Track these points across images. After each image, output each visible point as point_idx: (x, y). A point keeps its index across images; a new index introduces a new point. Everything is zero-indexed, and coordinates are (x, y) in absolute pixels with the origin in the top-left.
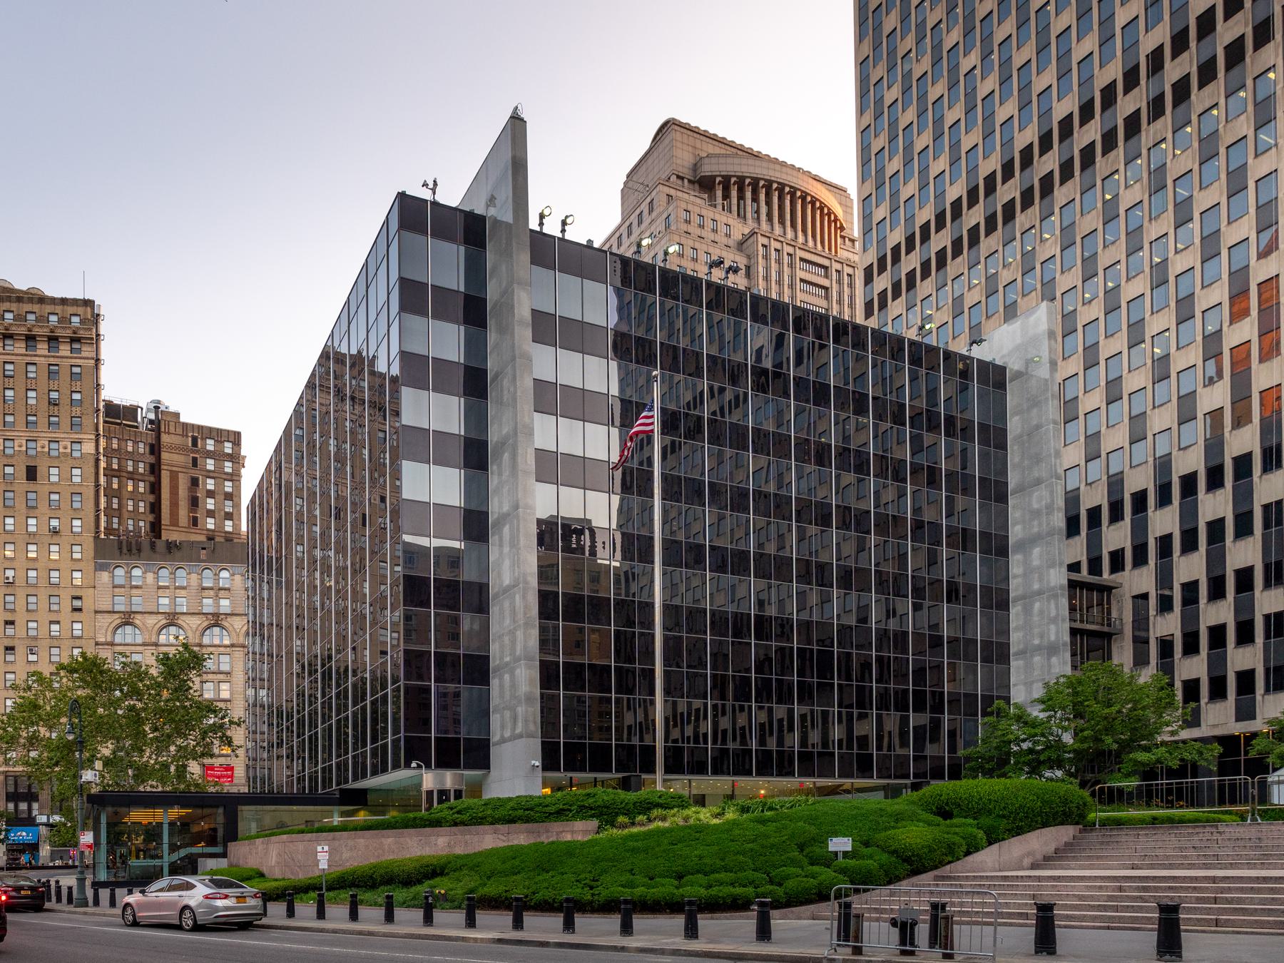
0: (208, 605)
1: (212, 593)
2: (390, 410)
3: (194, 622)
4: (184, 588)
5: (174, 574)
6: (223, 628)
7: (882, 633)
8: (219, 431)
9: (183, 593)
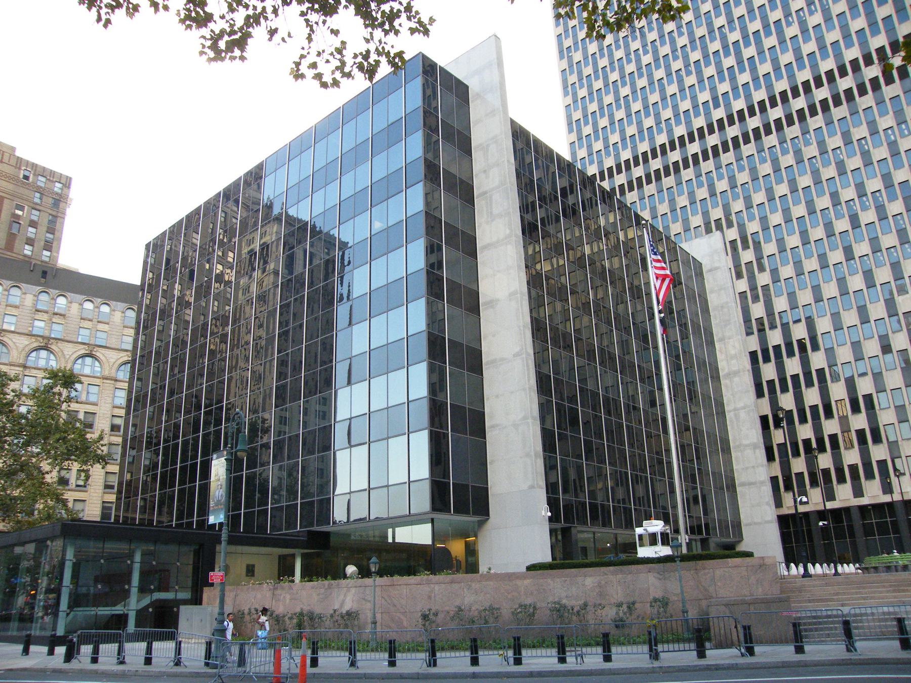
0: (40, 326)
1: (45, 317)
2: (242, 203)
3: (70, 351)
4: (16, 307)
5: (8, 291)
6: (50, 351)
7: (279, 457)
8: (52, 173)
9: (14, 311)
